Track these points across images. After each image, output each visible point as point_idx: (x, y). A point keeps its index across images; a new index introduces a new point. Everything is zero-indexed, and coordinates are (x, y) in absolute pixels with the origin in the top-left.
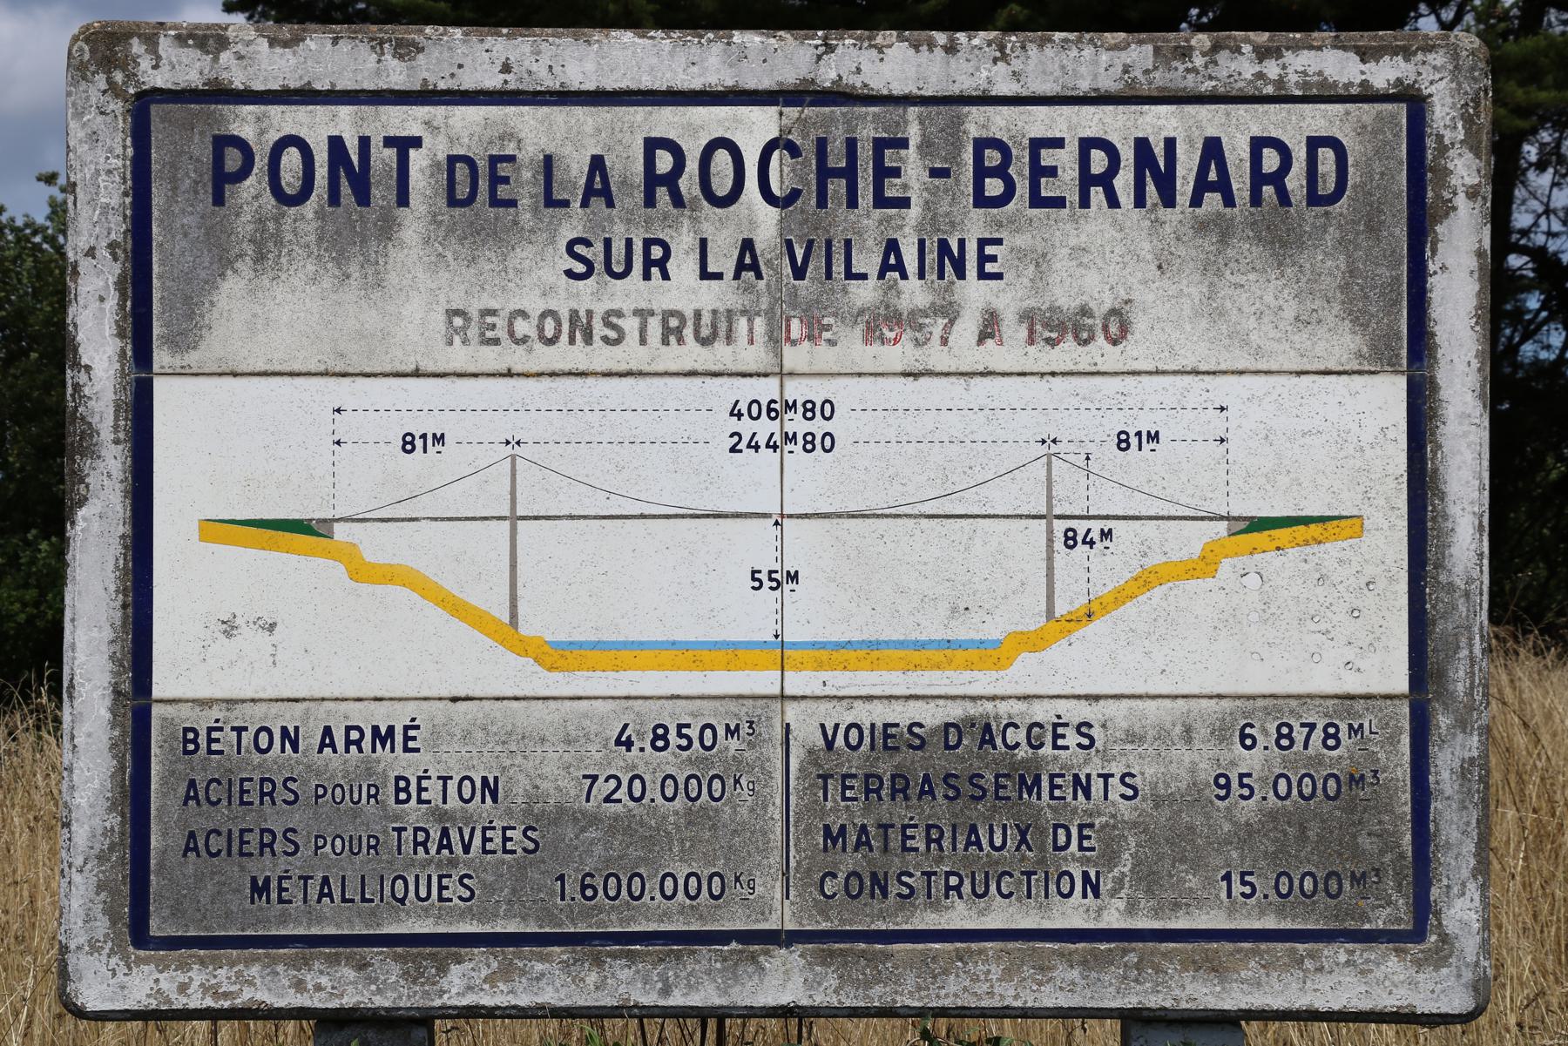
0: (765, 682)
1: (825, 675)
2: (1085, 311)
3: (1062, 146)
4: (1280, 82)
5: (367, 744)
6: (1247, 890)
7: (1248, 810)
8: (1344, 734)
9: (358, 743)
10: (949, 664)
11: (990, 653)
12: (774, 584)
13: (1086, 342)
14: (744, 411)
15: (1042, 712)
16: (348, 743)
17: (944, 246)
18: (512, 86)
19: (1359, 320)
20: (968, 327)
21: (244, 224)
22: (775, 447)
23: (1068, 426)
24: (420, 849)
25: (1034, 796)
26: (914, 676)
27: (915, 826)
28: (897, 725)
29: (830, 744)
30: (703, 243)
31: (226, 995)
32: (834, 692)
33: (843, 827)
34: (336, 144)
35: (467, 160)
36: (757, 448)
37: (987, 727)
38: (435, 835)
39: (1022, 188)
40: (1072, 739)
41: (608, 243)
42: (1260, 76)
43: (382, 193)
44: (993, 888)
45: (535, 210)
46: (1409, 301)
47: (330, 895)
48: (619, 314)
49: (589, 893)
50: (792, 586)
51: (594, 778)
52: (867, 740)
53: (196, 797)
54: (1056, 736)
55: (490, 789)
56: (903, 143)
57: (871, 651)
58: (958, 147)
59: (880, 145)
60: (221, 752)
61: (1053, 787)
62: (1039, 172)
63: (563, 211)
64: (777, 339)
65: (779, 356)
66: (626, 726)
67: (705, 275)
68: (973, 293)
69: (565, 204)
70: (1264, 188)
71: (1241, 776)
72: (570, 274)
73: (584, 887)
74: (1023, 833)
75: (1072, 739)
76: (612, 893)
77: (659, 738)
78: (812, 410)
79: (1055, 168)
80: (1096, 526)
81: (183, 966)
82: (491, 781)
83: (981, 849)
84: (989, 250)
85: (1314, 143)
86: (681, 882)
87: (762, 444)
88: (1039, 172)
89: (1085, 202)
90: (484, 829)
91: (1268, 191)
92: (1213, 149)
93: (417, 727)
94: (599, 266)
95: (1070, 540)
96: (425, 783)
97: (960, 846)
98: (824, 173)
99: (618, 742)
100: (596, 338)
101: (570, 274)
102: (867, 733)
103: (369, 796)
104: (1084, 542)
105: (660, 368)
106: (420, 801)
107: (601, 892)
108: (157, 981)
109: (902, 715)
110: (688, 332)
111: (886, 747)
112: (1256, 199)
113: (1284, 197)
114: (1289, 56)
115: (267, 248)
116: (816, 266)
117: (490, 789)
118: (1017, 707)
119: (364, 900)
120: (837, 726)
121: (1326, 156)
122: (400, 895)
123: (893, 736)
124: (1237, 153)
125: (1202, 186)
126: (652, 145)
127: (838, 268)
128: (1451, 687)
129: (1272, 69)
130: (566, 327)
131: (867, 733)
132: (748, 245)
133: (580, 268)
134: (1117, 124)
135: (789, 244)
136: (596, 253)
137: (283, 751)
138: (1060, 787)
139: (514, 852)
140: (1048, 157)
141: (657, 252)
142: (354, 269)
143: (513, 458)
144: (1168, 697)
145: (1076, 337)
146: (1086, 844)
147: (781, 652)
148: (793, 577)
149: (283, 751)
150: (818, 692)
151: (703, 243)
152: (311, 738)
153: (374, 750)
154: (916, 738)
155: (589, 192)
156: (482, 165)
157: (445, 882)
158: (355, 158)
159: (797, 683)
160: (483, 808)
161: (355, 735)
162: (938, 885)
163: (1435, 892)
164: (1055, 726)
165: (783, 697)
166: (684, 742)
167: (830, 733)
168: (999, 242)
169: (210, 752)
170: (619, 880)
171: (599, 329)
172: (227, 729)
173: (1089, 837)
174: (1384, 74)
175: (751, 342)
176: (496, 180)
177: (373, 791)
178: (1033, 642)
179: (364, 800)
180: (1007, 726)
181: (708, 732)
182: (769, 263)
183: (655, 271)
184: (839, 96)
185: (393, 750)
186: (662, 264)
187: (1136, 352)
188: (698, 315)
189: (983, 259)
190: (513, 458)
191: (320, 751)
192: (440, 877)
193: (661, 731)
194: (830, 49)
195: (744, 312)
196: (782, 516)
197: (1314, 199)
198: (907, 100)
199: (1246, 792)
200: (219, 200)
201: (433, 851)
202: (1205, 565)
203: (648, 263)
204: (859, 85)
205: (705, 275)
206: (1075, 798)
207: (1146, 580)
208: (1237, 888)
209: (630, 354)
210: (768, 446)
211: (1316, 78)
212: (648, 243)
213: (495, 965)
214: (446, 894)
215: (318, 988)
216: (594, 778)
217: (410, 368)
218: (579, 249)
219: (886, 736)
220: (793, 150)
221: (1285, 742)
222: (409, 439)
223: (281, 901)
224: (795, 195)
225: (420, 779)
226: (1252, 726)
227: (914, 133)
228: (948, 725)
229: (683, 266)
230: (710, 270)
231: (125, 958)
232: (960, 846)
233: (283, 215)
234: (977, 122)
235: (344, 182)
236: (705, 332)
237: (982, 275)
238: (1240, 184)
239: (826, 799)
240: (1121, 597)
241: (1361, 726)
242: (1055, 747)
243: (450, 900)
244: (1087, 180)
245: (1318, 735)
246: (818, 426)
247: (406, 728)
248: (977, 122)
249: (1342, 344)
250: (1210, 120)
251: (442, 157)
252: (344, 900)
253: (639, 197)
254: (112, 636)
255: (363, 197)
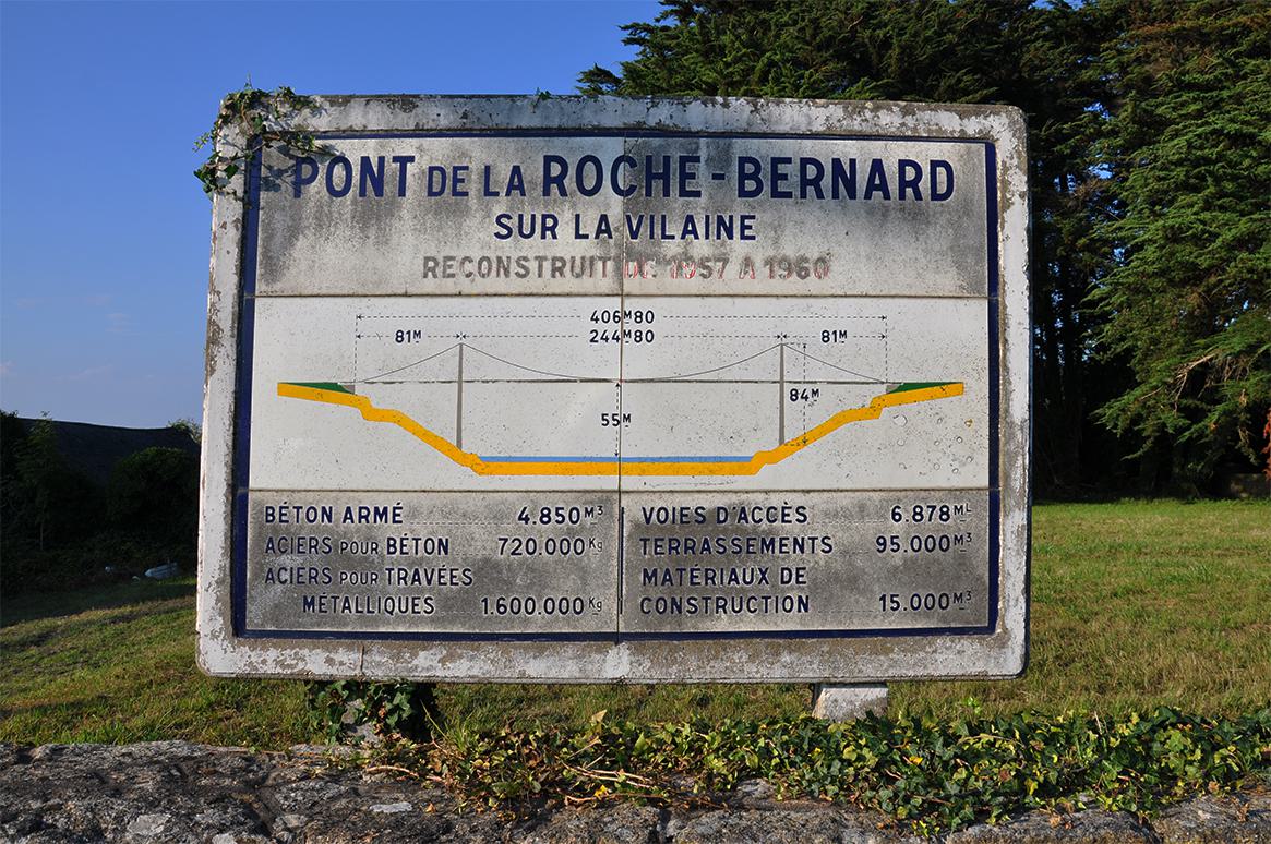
0: (609, 482)
1: (646, 478)
2: (804, 259)
3: (790, 162)
4: (915, 129)
5: (371, 518)
6: (895, 606)
7: (897, 559)
8: (951, 512)
9: (366, 517)
10: (720, 472)
11: (743, 464)
12: (616, 422)
13: (803, 278)
14: (600, 317)
15: (776, 501)
16: (361, 517)
17: (720, 220)
18: (468, 126)
19: (960, 266)
20: (733, 269)
21: (309, 208)
22: (618, 339)
23: (793, 328)
24: (402, 581)
25: (770, 552)
26: (699, 478)
27: (699, 570)
28: (688, 508)
29: (648, 520)
30: (578, 216)
31: (289, 666)
32: (651, 489)
33: (655, 570)
34: (365, 161)
35: (441, 170)
36: (607, 339)
37: (743, 510)
38: (411, 573)
39: (767, 188)
40: (793, 516)
41: (521, 217)
42: (903, 125)
43: (390, 188)
44: (745, 607)
45: (479, 199)
46: (989, 256)
47: (349, 608)
48: (525, 259)
49: (502, 609)
50: (627, 423)
51: (506, 540)
52: (671, 516)
53: (273, 548)
54: (784, 515)
55: (444, 546)
56: (697, 159)
57: (674, 463)
58: (728, 162)
59: (683, 161)
60: (287, 522)
61: (782, 545)
62: (777, 177)
63: (495, 198)
64: (620, 273)
65: (621, 284)
66: (525, 508)
67: (578, 236)
68: (738, 247)
69: (497, 194)
70: (907, 189)
71: (892, 538)
72: (498, 235)
73: (499, 606)
74: (763, 574)
75: (793, 516)
76: (515, 610)
77: (545, 516)
78: (640, 317)
79: (786, 175)
80: (809, 388)
81: (265, 648)
82: (444, 541)
83: (738, 583)
84: (747, 222)
85: (934, 164)
86: (557, 604)
87: (610, 337)
88: (777, 177)
89: (803, 195)
90: (440, 570)
91: (909, 191)
92: (877, 166)
93: (401, 508)
94: (515, 231)
95: (794, 396)
96: (405, 542)
97: (726, 581)
98: (650, 177)
99: (520, 518)
100: (512, 274)
101: (498, 235)
102: (670, 513)
103: (373, 549)
104: (802, 397)
105: (550, 292)
106: (402, 553)
107: (509, 609)
108: (249, 657)
109: (692, 502)
110: (567, 270)
111: (682, 522)
112: (902, 196)
113: (918, 196)
114: (919, 115)
115: (323, 221)
116: (644, 231)
117: (444, 546)
118: (761, 496)
119: (369, 611)
120: (652, 509)
121: (941, 171)
122: (390, 609)
123: (687, 515)
124: (891, 169)
125: (871, 187)
126: (548, 160)
127: (658, 231)
128: (1013, 483)
129: (910, 121)
130: (494, 266)
131: (670, 513)
132: (604, 218)
133: (505, 232)
134: (825, 151)
135: (628, 218)
136: (513, 223)
137: (323, 521)
138: (786, 545)
139: (457, 584)
140: (782, 168)
141: (550, 223)
142: (372, 232)
143: (461, 345)
144: (851, 490)
145: (799, 275)
146: (800, 579)
147: (619, 462)
148: (627, 418)
149: (323, 521)
150: (641, 488)
151: (578, 216)
152: (341, 512)
153: (375, 522)
154: (701, 517)
155: (511, 187)
156: (449, 172)
157: (416, 601)
158: (375, 169)
159: (629, 482)
160: (439, 559)
161: (364, 512)
162: (712, 605)
163: (1000, 606)
164: (784, 508)
165: (618, 459)
166: (560, 519)
167: (648, 513)
168: (753, 217)
169: (281, 521)
170: (520, 602)
171: (514, 268)
172: (291, 508)
173: (802, 576)
174: (973, 126)
175: (604, 274)
176: (456, 180)
177: (374, 546)
178: (772, 458)
179: (369, 552)
180: (755, 509)
181: (575, 512)
182: (617, 229)
183: (548, 233)
184: (661, 131)
185: (386, 522)
186: (552, 229)
187: (835, 280)
188: (573, 259)
189: (744, 227)
190: (461, 345)
191: (344, 522)
192: (414, 599)
193: (546, 512)
194: (655, 105)
195: (600, 258)
196: (621, 381)
197: (935, 196)
198: (698, 135)
199: (895, 547)
200: (298, 194)
201: (409, 583)
202: (874, 410)
203: (544, 229)
204: (671, 125)
205: (578, 236)
206: (795, 552)
207: (837, 421)
208: (889, 604)
209: (531, 282)
210: (613, 338)
211: (934, 127)
212: (544, 217)
213: (445, 652)
214: (416, 609)
215: (342, 664)
216: (506, 540)
217: (402, 291)
218: (504, 221)
219: (682, 515)
220: (632, 163)
221: (918, 517)
222: (400, 334)
223: (321, 611)
224: (632, 189)
225: (402, 539)
226: (899, 508)
227: (703, 154)
228: (719, 509)
229: (565, 230)
230: (581, 233)
231: (231, 642)
232: (726, 581)
233: (332, 201)
234: (741, 147)
235: (369, 183)
236: (577, 270)
237: (743, 237)
238: (893, 186)
239: (645, 553)
240: (823, 430)
241: (961, 507)
242: (783, 521)
243: (419, 612)
244: (805, 182)
245: (937, 512)
246: (644, 327)
247: (395, 509)
248: (741, 147)
249: (949, 280)
250: (876, 149)
251: (426, 167)
252: (357, 611)
253: (540, 189)
254: (227, 452)
255: (379, 192)
